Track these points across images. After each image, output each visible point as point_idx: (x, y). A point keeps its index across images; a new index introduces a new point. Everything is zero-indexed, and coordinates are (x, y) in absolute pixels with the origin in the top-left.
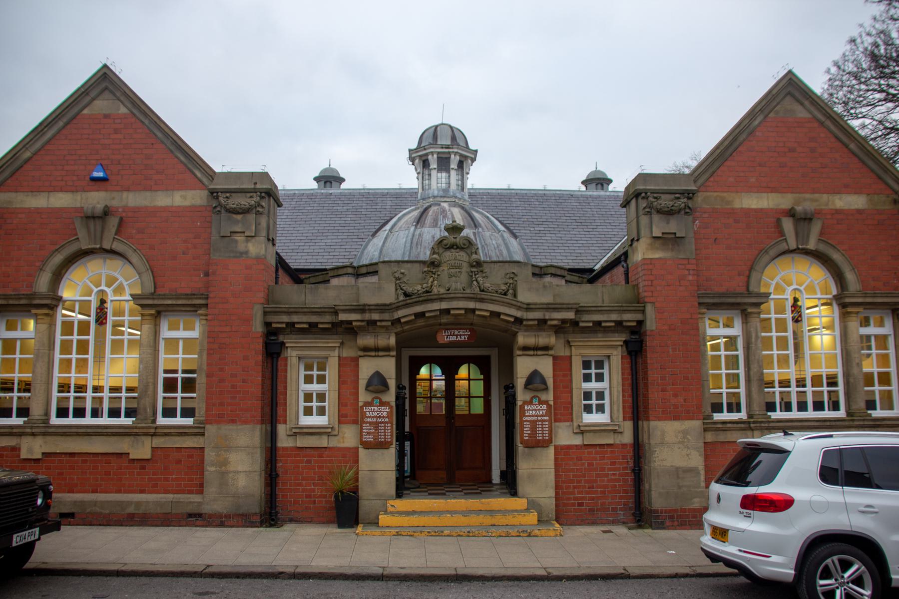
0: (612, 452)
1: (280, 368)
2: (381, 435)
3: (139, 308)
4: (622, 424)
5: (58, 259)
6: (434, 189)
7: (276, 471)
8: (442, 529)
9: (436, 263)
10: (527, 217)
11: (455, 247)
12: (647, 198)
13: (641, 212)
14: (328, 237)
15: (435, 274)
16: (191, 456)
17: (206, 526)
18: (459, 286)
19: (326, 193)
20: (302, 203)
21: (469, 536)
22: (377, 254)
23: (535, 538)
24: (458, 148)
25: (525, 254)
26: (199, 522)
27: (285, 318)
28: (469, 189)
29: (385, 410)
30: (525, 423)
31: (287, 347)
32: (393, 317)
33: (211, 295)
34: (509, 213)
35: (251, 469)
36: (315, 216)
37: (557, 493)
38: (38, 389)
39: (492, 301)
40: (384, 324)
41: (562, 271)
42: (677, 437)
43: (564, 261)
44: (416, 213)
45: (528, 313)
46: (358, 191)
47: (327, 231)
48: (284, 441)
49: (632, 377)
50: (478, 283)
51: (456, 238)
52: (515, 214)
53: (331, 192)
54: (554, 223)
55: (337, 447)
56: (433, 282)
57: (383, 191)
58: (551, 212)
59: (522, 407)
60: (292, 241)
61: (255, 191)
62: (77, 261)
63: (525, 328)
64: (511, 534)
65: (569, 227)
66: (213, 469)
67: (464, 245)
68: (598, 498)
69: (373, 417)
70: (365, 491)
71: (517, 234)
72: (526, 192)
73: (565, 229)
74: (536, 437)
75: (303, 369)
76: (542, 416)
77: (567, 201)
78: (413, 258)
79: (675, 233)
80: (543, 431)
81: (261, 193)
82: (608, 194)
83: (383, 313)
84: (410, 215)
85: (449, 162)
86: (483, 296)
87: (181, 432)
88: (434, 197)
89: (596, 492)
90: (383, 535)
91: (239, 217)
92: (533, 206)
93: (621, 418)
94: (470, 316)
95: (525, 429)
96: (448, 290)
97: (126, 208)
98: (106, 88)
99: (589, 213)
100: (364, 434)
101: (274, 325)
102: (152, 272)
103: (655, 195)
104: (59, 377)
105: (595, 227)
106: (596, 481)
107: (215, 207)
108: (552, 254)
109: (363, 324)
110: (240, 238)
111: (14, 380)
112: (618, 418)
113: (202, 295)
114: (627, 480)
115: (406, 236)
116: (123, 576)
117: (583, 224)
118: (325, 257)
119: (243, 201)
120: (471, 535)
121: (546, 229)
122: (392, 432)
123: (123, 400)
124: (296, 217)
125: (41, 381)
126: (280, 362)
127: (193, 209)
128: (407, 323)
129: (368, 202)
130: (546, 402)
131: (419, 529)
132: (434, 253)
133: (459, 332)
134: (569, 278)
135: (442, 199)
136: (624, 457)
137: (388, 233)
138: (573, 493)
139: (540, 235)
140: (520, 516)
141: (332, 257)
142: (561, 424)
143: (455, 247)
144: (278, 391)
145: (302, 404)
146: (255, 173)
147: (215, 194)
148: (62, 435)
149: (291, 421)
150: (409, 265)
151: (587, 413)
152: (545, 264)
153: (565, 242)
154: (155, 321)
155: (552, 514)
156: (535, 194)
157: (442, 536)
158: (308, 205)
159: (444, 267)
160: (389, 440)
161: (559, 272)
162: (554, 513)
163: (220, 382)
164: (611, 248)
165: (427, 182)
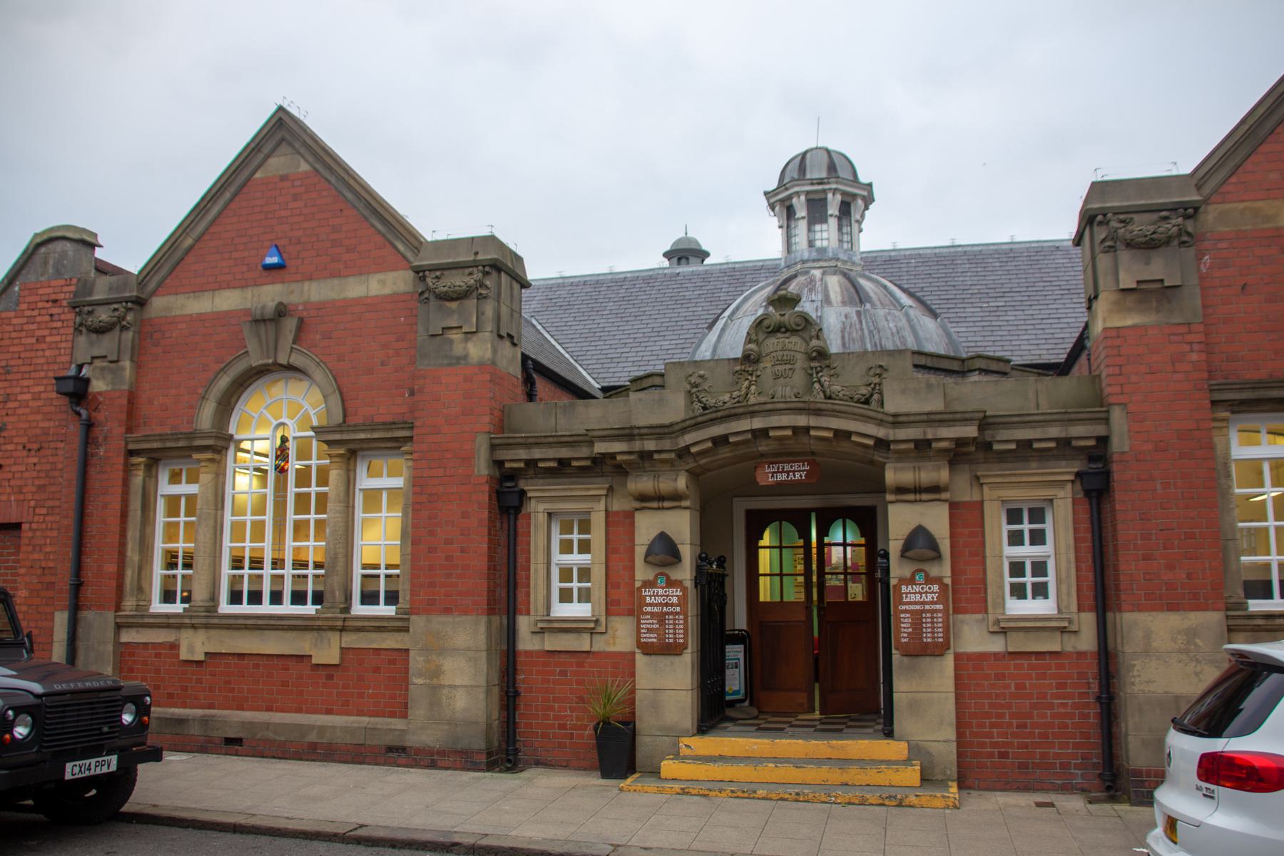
0: (1059, 666)
1: (520, 530)
3: (325, 447)
4: (1075, 617)
5: (224, 382)
7: (514, 687)
8: (752, 786)
9: (752, 357)
10: (978, 287)
11: (783, 330)
12: (1108, 223)
13: (1098, 249)
14: (666, 338)
15: (751, 375)
16: (392, 662)
17: (412, 767)
19: (671, 274)
21: (797, 801)
23: (908, 809)
24: (837, 183)
25: (951, 342)
26: (403, 760)
27: (523, 454)
30: (902, 615)
31: (530, 498)
33: (417, 423)
34: (949, 284)
35: (473, 683)
37: (960, 734)
38: (201, 562)
39: (835, 413)
40: (664, 456)
42: (1174, 640)
45: (897, 430)
46: (718, 267)
48: (527, 642)
49: (1093, 536)
50: (822, 386)
55: (604, 652)
56: (748, 388)
57: (756, 264)
58: (1020, 276)
59: (898, 587)
60: (613, 347)
61: (475, 264)
62: (251, 384)
63: (897, 456)
64: (870, 801)
66: (420, 681)
67: (798, 325)
69: (656, 605)
70: (645, 721)
71: (938, 311)
72: (980, 248)
73: (1041, 302)
74: (921, 639)
75: (558, 531)
76: (932, 603)
79: (1162, 281)
81: (484, 266)
87: (379, 625)
88: (804, 262)
90: (660, 792)
91: (454, 305)
92: (991, 269)
93: (1074, 607)
94: (805, 439)
95: (902, 625)
97: (307, 305)
98: (283, 139)
100: (643, 631)
101: (507, 465)
102: (341, 394)
103: (1122, 217)
104: (231, 548)
106: (1030, 716)
107: (422, 293)
108: (1014, 343)
109: (632, 457)
110: (456, 336)
111: (178, 552)
112: (1068, 607)
113: (405, 423)
114: (1087, 716)
116: (241, 833)
117: (1072, 291)
119: (458, 281)
120: (801, 799)
122: (686, 629)
123: (310, 579)
125: (205, 552)
126: (520, 522)
127: (394, 298)
128: (702, 453)
129: (732, 281)
130: (938, 580)
131: (720, 785)
133: (791, 467)
136: (1082, 675)
137: (726, 321)
138: (990, 735)
139: (998, 313)
140: (891, 771)
144: (519, 565)
145: (556, 585)
146: (477, 238)
147: (421, 274)
148: (228, 629)
149: (537, 610)
154: (348, 464)
155: (951, 770)
156: (996, 250)
157: (754, 798)
159: (767, 363)
160: (682, 641)
162: (955, 769)
163: (429, 552)
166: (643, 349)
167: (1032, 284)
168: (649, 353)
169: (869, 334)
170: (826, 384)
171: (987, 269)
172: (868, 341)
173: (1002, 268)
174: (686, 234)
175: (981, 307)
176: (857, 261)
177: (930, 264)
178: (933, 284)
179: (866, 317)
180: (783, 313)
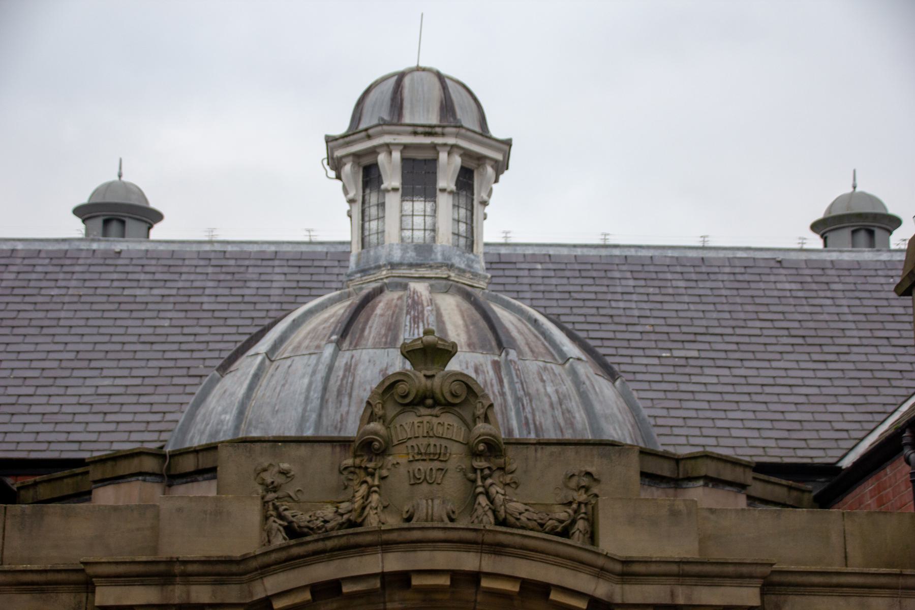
6: (391, 245)
9: (376, 445)
10: (652, 321)
11: (429, 401)
14: (105, 373)
15: (372, 475)
18: (438, 509)
19: (105, 251)
20: (34, 276)
22: (229, 418)
24: (457, 135)
25: (639, 422)
28: (486, 244)
32: (251, 594)
34: (602, 311)
36: (70, 314)
39: (526, 552)
41: (739, 470)
44: (340, 310)
45: (627, 587)
46: (195, 248)
47: (102, 355)
50: (491, 501)
51: (433, 376)
52: (621, 312)
53: (118, 247)
54: (727, 339)
56: (366, 497)
57: (265, 248)
58: (719, 307)
65: (770, 348)
67: (454, 396)
72: (650, 253)
73: (759, 356)
77: (764, 278)
78: (327, 431)
82: (884, 257)
83: (222, 583)
84: (326, 314)
85: (435, 173)
86: (502, 538)
88: (393, 266)
92: (671, 291)
96: (409, 520)
99: (826, 309)
105: (845, 349)
108: (719, 423)
115: (310, 370)
117: (810, 340)
118: (91, 427)
121: (703, 354)
124: (13, 315)
129: (222, 277)
132: (372, 418)
134: (758, 489)
135: (414, 272)
137: (262, 362)
139: (687, 370)
141: (112, 427)
143: (429, 401)
150: (303, 450)
152: (700, 449)
153: (759, 389)
158: (52, 284)
159: (399, 457)
161: (728, 473)
164: (890, 409)
165: (374, 225)
166: (61, 391)
167: (742, 323)
168: (74, 400)
169: (515, 404)
170: (499, 499)
171: (664, 291)
172: (513, 414)
173: (690, 292)
174: (120, 176)
175: (659, 357)
176: (481, 272)
177: (568, 274)
178: (575, 311)
179: (509, 374)
180: (429, 373)
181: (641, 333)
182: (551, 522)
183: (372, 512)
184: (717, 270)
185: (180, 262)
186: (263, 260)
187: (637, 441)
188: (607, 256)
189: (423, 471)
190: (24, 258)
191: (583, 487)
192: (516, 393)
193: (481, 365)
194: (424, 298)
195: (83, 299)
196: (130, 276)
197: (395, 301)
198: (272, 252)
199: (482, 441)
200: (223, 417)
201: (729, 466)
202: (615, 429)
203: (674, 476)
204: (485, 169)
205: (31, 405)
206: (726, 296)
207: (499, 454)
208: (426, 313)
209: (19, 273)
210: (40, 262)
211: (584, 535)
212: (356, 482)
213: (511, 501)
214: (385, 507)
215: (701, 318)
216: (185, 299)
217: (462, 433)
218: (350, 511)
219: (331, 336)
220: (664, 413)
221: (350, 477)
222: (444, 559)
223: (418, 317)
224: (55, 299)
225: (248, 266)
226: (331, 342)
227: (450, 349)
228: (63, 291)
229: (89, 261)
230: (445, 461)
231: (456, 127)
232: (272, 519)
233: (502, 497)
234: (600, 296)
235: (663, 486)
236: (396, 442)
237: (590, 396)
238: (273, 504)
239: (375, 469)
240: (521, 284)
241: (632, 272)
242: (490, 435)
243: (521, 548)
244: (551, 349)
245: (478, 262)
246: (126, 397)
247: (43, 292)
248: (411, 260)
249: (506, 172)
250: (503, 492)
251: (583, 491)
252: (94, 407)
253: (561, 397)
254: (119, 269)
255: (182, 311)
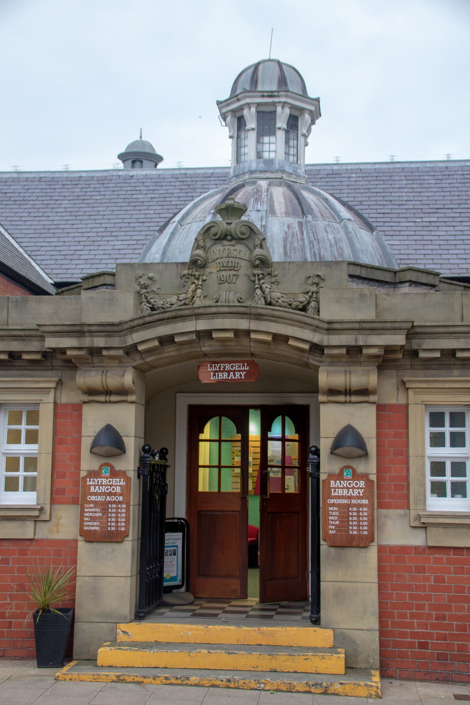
2: (111, 522)
8: (185, 673)
9: (199, 262)
11: (229, 238)
14: (119, 238)
15: (198, 279)
18: (232, 297)
20: (89, 190)
21: (228, 687)
24: (286, 96)
25: (385, 254)
29: (120, 482)
30: (330, 509)
32: (125, 342)
34: (386, 198)
36: (105, 209)
37: (382, 624)
40: (112, 353)
43: (461, 266)
45: (331, 337)
46: (171, 172)
52: (397, 198)
53: (131, 173)
54: (454, 210)
56: (195, 291)
57: (207, 171)
58: (453, 194)
59: (327, 482)
63: (330, 360)
67: (243, 234)
68: (454, 637)
69: (100, 494)
71: (374, 224)
74: (347, 531)
76: (358, 497)
80: (360, 521)
83: (110, 336)
85: (275, 119)
88: (251, 172)
89: (450, 627)
92: (426, 186)
94: (245, 341)
95: (330, 518)
96: (217, 302)
106: (449, 608)
108: (444, 257)
120: (232, 685)
121: (440, 220)
122: (127, 518)
124: (77, 210)
129: (183, 187)
130: (365, 477)
135: (263, 175)
137: (177, 226)
138: (410, 625)
139: (430, 229)
140: (317, 659)
142: (391, 512)
151: (439, 496)
152: (406, 266)
155: (374, 658)
157: (187, 685)
158: (98, 193)
159: (212, 269)
160: (123, 529)
162: (377, 657)
167: (464, 202)
169: (309, 245)
170: (267, 291)
172: (308, 250)
173: (437, 186)
174: (141, 137)
176: (302, 174)
181: (406, 209)
182: (295, 303)
183: (198, 299)
184: (454, 173)
185: (162, 180)
186: (205, 177)
187: (382, 264)
188: (392, 168)
189: (225, 276)
190: (85, 181)
191: (315, 283)
192: (310, 239)
193: (292, 224)
194: (263, 188)
195: (112, 201)
196: (137, 188)
197: (249, 191)
198: (210, 173)
199: (258, 259)
200: (155, 256)
201: (425, 274)
202: (367, 258)
203: (393, 281)
204: (304, 116)
205: (81, 255)
206: (457, 187)
207: (268, 266)
208: (263, 196)
209: (82, 188)
210: (93, 182)
211: (314, 310)
212: (189, 283)
213: (274, 292)
214: (205, 297)
215: (442, 200)
216: (163, 199)
217: (248, 255)
218: (186, 299)
219: (211, 210)
220: (414, 252)
221: (186, 280)
222: (229, 323)
223: (258, 199)
224: (98, 201)
225: (197, 181)
226: (211, 214)
227: (242, 208)
228: (102, 197)
229: (117, 181)
230: (238, 271)
231: (285, 91)
232: (144, 303)
233: (269, 290)
234: (386, 190)
235: (386, 287)
236: (210, 261)
237: (354, 240)
238: (145, 295)
239: (199, 276)
240: (343, 185)
241: (405, 176)
242: (262, 255)
243: (271, 316)
244: (334, 215)
245: (300, 169)
246: (128, 250)
247: (93, 198)
248: (262, 169)
249: (320, 118)
250: (269, 287)
251: (315, 285)
252: (112, 255)
253: (337, 240)
254: (132, 185)
255: (161, 205)
